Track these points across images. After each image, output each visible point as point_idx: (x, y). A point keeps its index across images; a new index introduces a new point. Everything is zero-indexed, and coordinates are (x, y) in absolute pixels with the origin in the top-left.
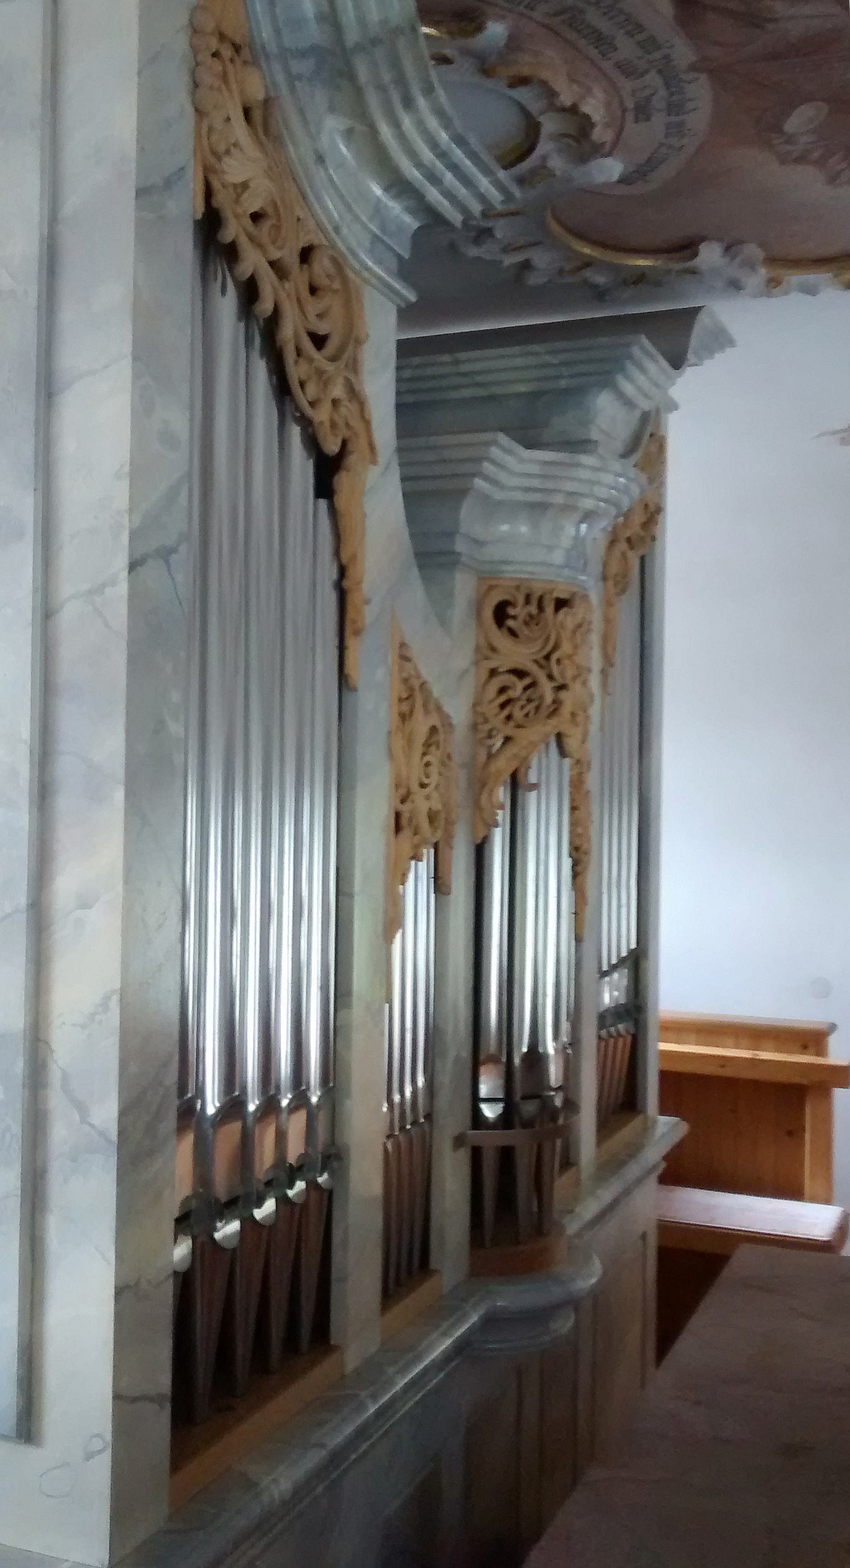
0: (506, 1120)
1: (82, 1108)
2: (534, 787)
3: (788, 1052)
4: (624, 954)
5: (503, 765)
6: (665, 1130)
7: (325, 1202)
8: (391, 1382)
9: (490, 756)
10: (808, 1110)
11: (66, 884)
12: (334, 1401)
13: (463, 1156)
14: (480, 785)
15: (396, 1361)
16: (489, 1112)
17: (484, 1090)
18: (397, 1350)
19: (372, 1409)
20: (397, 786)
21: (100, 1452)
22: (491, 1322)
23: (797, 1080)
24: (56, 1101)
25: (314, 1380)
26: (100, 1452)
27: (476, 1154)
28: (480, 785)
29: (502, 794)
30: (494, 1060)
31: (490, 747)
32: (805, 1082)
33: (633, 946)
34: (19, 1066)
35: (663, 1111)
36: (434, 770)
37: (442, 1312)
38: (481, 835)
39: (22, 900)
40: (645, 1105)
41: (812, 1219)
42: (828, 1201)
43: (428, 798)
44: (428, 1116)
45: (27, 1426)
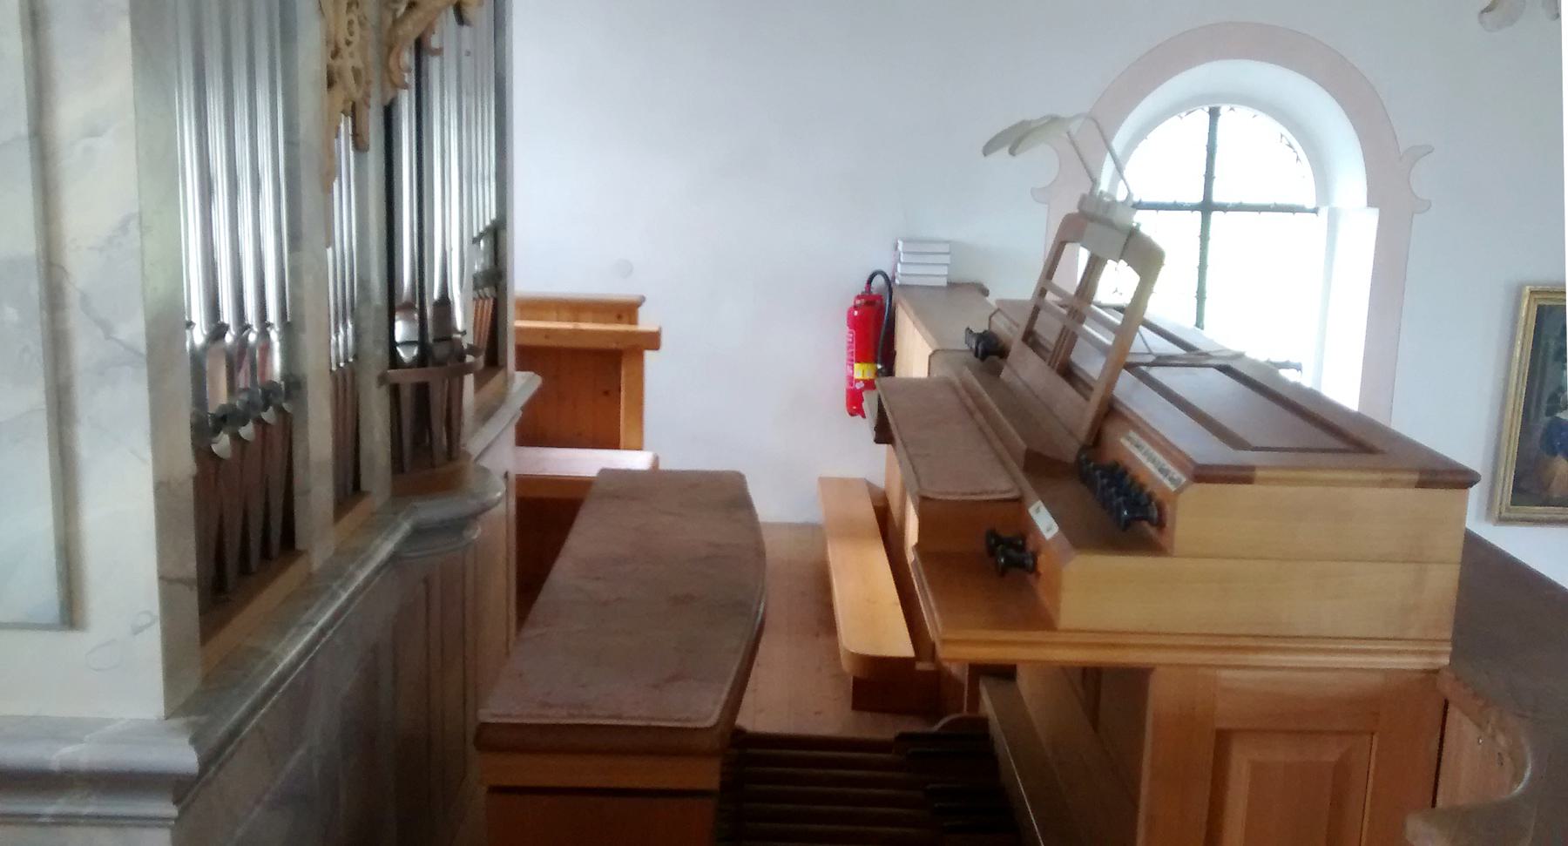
0: (422, 361)
1: (107, 329)
2: (439, 52)
3: (605, 322)
4: (488, 223)
5: (410, 30)
6: (523, 384)
7: (288, 428)
8: (352, 576)
9: (396, 22)
10: (623, 373)
11: (70, 113)
12: (312, 591)
13: (384, 390)
14: (389, 47)
15: (349, 566)
16: (404, 354)
17: (399, 337)
18: (351, 554)
19: (344, 596)
20: (328, 42)
21: (149, 625)
22: (419, 533)
23: (613, 346)
24: (75, 319)
25: (289, 579)
26: (149, 625)
27: (395, 391)
28: (389, 47)
29: (408, 58)
30: (408, 307)
31: (396, 10)
32: (620, 347)
33: (494, 216)
34: (35, 288)
35: (521, 366)
36: (356, 27)
37: (377, 525)
38: (389, 99)
39: (24, 129)
40: (505, 365)
41: (634, 460)
42: (640, 448)
43: (351, 55)
44: (355, 357)
45: (70, 613)
